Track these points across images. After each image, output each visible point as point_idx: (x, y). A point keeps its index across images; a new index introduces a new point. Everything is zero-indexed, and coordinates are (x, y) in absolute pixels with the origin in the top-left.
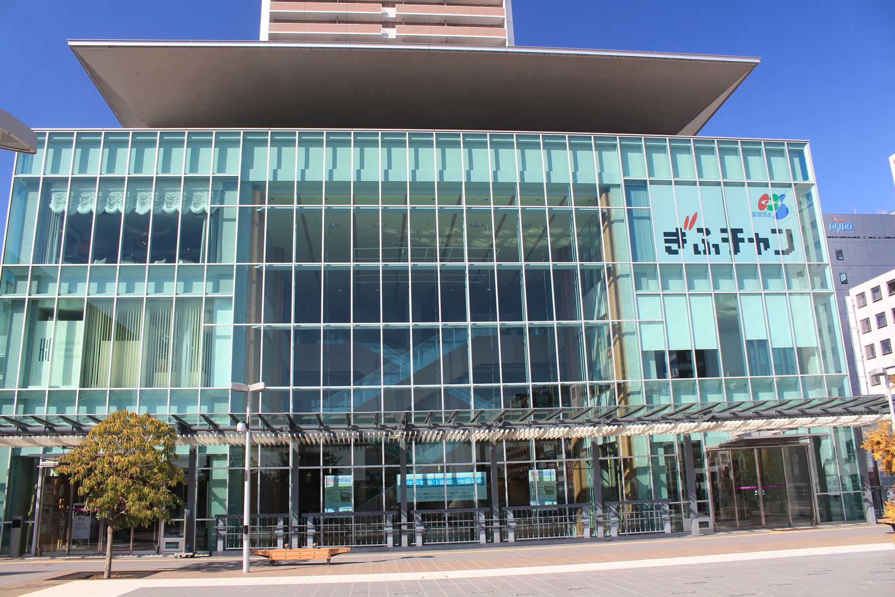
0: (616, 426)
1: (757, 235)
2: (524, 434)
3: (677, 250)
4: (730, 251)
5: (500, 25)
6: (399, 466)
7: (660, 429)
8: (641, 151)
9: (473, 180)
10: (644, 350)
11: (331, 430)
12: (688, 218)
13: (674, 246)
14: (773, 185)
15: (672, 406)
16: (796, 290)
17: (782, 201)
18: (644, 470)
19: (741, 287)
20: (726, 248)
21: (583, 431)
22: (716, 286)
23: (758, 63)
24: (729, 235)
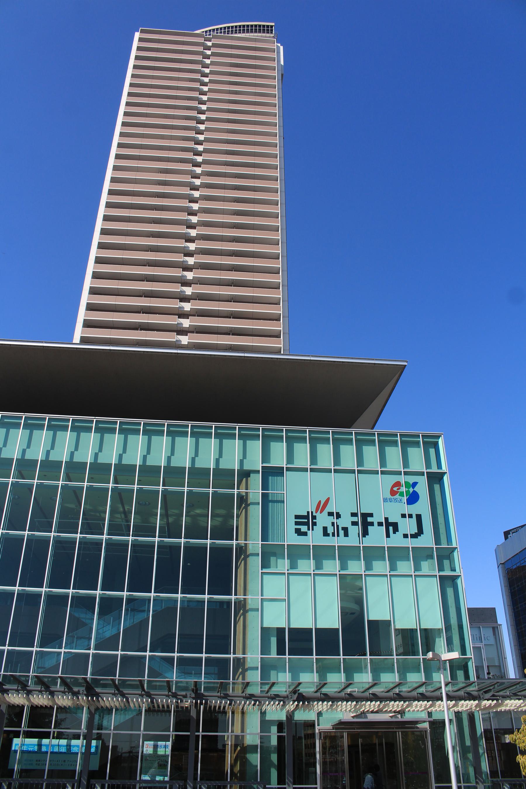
0: (495, 702)
1: (386, 519)
2: (318, 707)
3: (307, 532)
4: (359, 534)
5: (278, 336)
6: (189, 733)
7: (464, 706)
8: (419, 447)
9: (221, 467)
10: (264, 626)
11: (178, 697)
12: (320, 502)
13: (304, 528)
14: (406, 473)
15: (476, 683)
16: (424, 572)
17: (413, 488)
18: (253, 749)
19: (368, 567)
20: (354, 531)
21: (393, 706)
22: (343, 567)
23: (406, 365)
24: (359, 519)
